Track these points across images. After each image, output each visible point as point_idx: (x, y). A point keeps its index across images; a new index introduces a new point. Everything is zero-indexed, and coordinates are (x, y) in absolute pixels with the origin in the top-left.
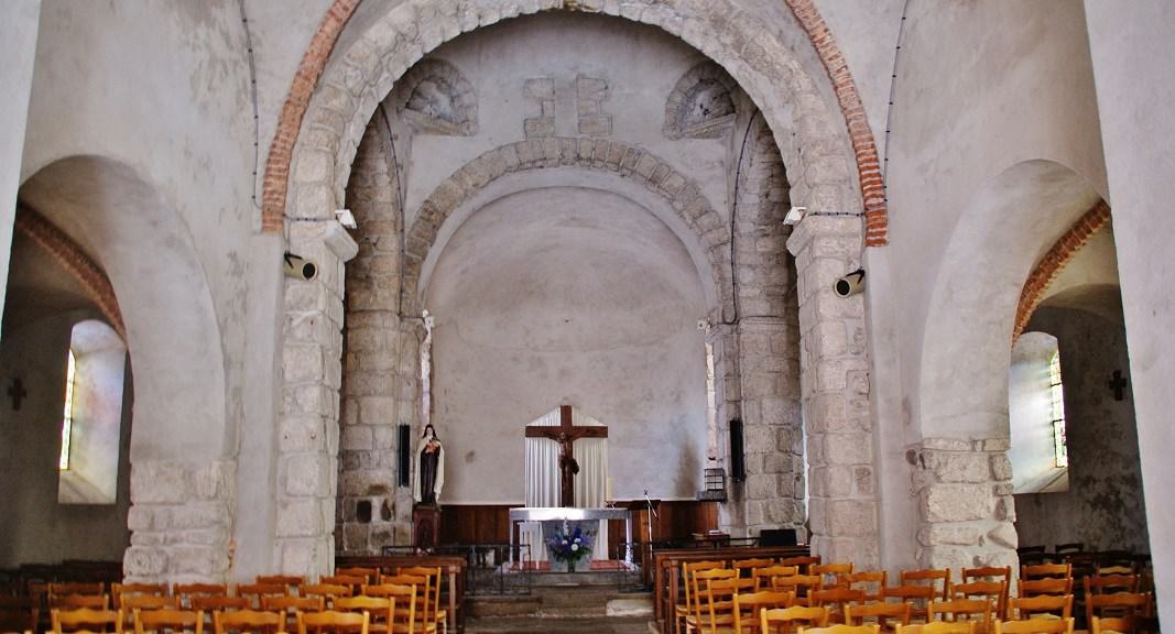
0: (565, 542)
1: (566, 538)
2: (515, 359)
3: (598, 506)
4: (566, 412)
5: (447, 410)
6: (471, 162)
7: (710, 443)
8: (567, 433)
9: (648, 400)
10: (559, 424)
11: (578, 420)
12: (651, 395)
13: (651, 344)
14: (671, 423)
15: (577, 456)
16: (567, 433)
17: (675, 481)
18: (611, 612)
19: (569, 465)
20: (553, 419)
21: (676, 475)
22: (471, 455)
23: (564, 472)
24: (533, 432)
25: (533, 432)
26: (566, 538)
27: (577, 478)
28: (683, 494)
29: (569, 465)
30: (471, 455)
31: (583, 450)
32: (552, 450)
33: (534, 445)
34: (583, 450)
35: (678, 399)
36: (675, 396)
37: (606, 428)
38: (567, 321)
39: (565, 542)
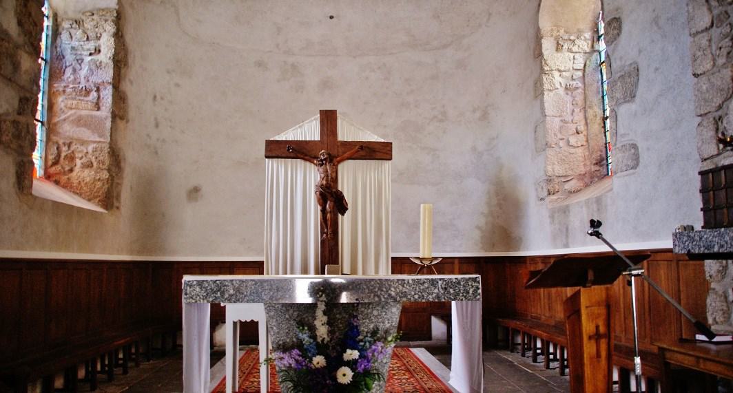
0: (319, 361)
1: (321, 349)
2: (260, 64)
3: (377, 272)
4: (329, 119)
5: (157, 126)
6: (316, 165)
7: (549, 168)
8: (329, 151)
9: (441, 121)
10: (317, 138)
11: (347, 132)
12: (444, 114)
13: (445, 47)
14: (474, 149)
15: (345, 186)
16: (329, 151)
17: (478, 228)
18: (329, 202)
19: (332, 201)
20: (310, 131)
21: (482, 221)
22: (194, 193)
23: (324, 211)
24: (277, 150)
25: (277, 150)
26: (321, 349)
27: (345, 221)
28: (493, 246)
29: (332, 201)
30: (194, 193)
31: (353, 178)
32: (308, 176)
33: (278, 169)
34: (353, 178)
35: (485, 116)
36: (478, 114)
37: (391, 143)
38: (331, 17)
39: (319, 361)
